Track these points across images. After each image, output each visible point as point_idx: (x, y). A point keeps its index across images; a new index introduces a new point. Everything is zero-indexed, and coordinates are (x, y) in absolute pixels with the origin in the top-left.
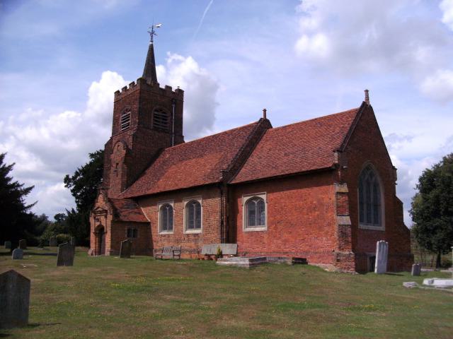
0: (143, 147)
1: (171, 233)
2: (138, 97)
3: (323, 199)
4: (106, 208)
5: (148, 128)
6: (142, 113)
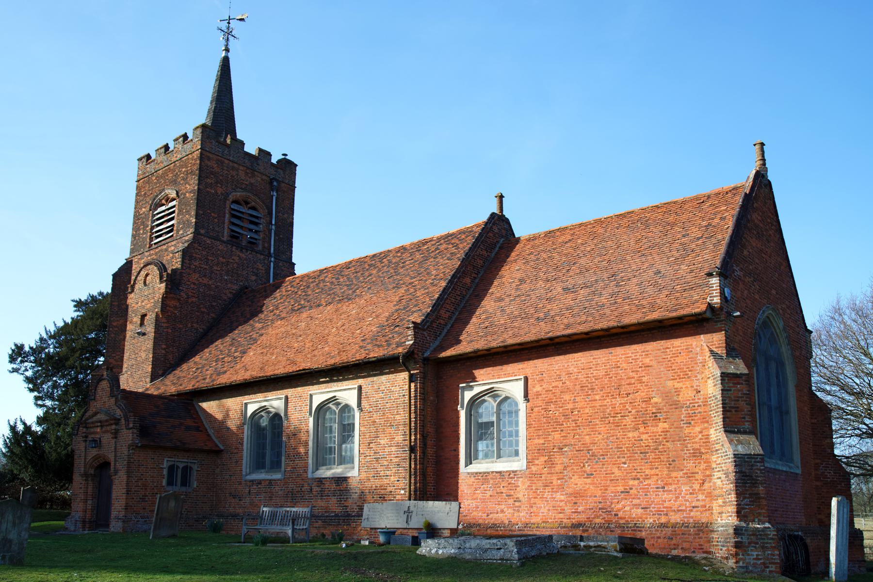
0: (206, 281)
1: (278, 476)
2: (196, 167)
3: (678, 391)
4: (118, 413)
5: (217, 239)
6: (206, 204)
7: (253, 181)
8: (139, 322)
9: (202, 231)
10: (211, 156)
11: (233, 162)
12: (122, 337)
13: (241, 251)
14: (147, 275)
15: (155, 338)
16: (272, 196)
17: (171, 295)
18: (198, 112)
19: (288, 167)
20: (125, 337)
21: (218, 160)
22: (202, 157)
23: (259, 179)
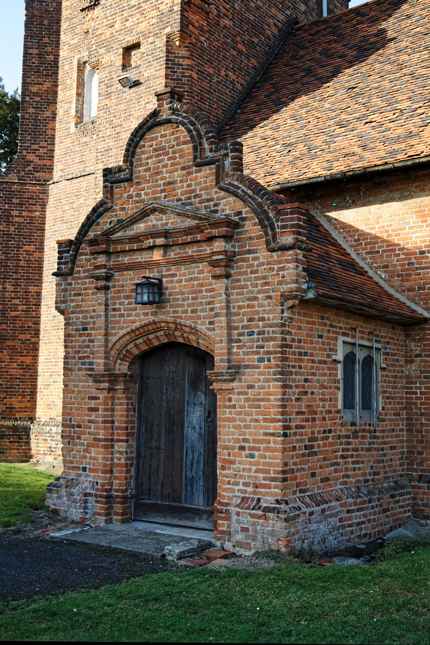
8: (119, 62)
12: (48, 114)
20: (54, 115)
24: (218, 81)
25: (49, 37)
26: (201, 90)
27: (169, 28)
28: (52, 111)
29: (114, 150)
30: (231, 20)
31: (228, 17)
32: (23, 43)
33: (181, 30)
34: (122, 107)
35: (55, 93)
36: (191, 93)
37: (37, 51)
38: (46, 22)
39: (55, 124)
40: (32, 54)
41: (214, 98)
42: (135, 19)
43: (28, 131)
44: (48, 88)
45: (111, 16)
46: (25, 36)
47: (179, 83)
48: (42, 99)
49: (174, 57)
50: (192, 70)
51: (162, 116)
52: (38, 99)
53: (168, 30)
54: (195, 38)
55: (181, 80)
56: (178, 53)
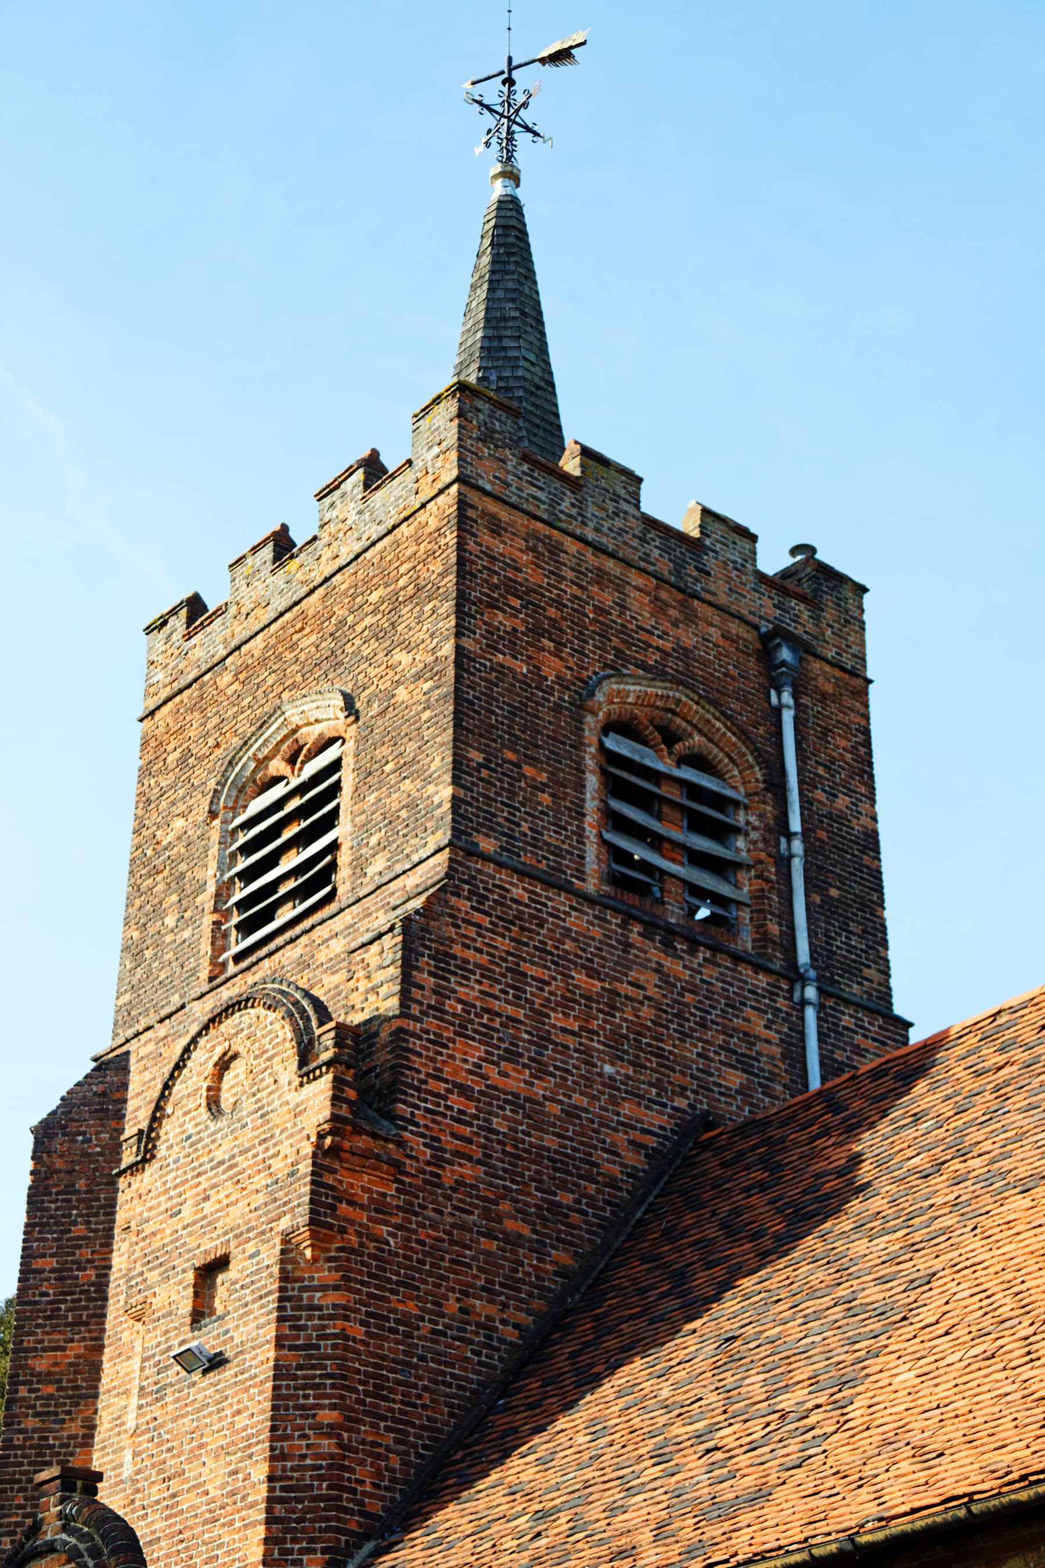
7: (688, 638)
8: (186, 1306)
9: (488, 845)
10: (504, 514)
11: (599, 549)
12: (74, 1428)
13: (667, 946)
14: (224, 1064)
15: (280, 1372)
16: (778, 711)
17: (361, 1142)
18: (439, 338)
19: (821, 588)
20: (91, 1427)
21: (534, 535)
22: (464, 519)
23: (714, 633)
24: (433, 1332)
25: (88, 1223)
26: (375, 1366)
27: (288, 1216)
28: (85, 1419)
29: (163, 1544)
30: (479, 1162)
31: (469, 1158)
32: (21, 1244)
33: (312, 1222)
34: (187, 1423)
35: (95, 1370)
36: (343, 1377)
37: (54, 1262)
38: (81, 1184)
39: (90, 1453)
40: (40, 1271)
41: (420, 1378)
42: (221, 1196)
43: (19, 1481)
44: (77, 1357)
45: (176, 1187)
46: (27, 1225)
47: (310, 1357)
48: (59, 1389)
49: (302, 1289)
50: (346, 1318)
51: (45, 1533)
52: (51, 1389)
53: (285, 1223)
54: (359, 1234)
55: (317, 1347)
56: (312, 1278)
